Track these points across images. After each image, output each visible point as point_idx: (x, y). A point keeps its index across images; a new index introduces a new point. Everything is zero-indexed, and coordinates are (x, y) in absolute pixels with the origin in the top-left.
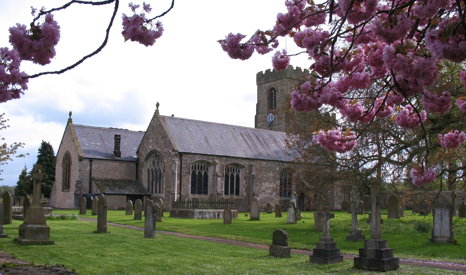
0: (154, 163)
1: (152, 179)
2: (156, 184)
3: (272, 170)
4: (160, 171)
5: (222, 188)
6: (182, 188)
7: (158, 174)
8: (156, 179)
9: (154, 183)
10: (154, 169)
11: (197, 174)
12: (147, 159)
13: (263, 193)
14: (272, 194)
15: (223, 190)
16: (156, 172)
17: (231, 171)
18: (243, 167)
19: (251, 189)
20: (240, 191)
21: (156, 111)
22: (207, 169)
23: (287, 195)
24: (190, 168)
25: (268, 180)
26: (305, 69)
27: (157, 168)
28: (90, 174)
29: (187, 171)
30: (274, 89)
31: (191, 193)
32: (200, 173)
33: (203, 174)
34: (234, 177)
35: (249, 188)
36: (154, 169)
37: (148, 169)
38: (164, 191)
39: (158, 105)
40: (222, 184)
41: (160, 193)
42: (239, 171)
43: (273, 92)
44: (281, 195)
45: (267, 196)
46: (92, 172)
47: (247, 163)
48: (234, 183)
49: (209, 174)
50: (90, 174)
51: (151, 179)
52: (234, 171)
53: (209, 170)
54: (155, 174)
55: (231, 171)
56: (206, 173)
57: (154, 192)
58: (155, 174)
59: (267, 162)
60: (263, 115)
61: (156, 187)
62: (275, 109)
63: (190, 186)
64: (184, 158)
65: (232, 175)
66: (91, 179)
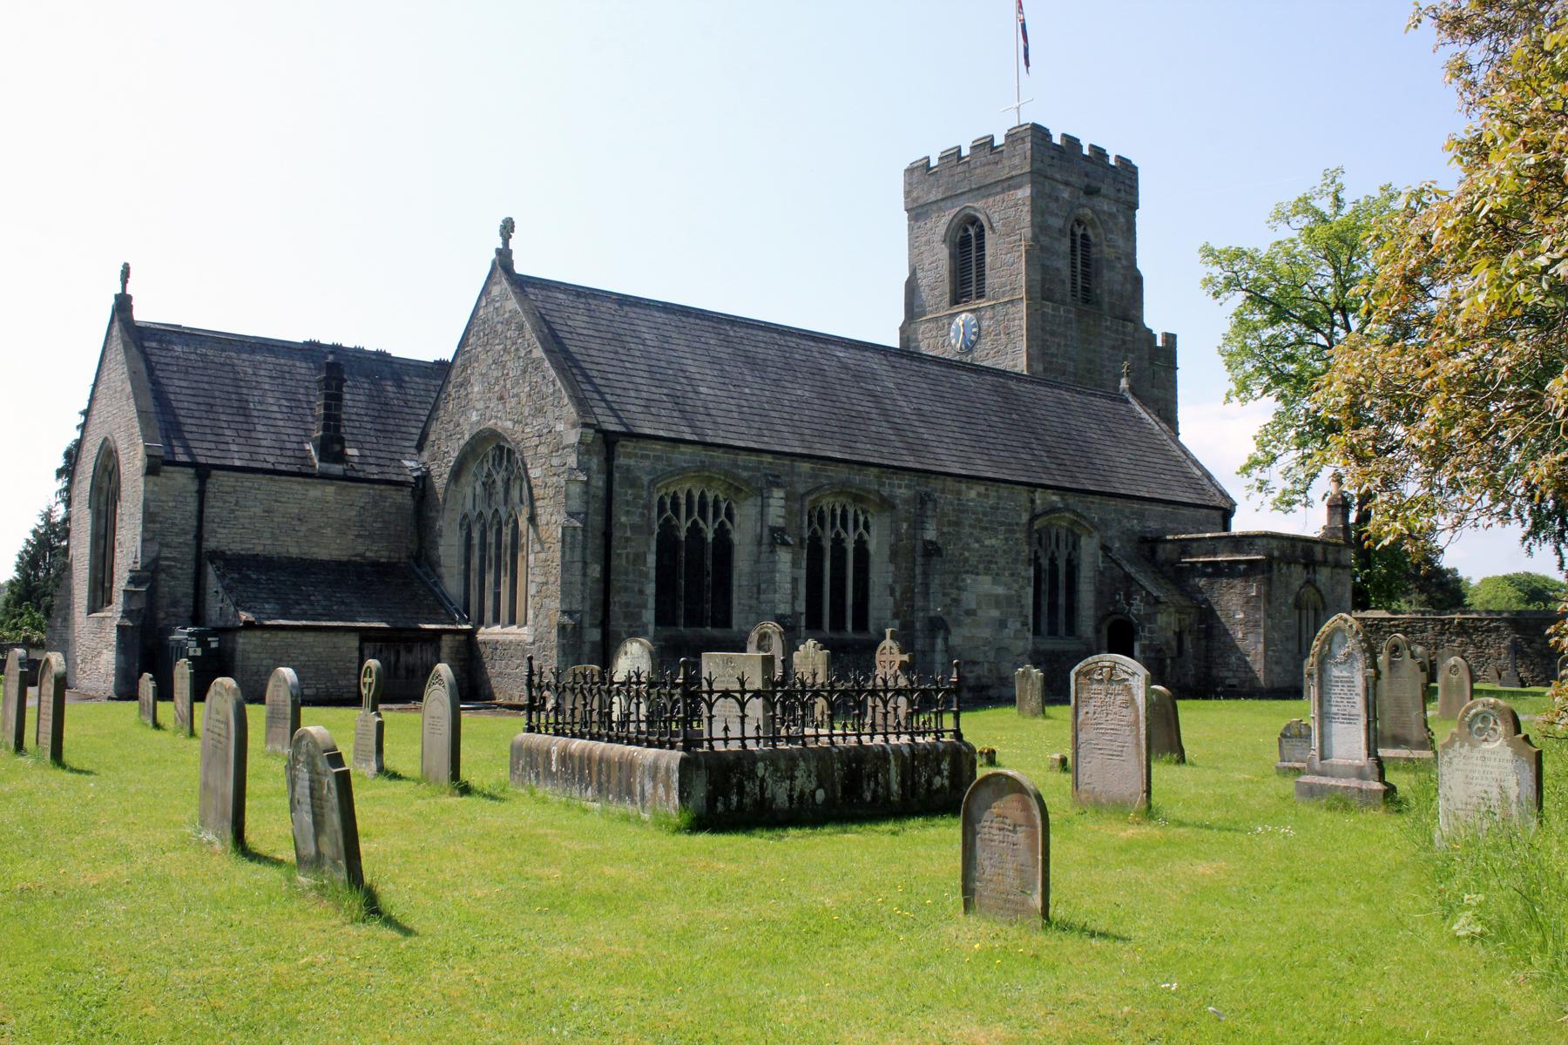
0: (488, 486)
1: (482, 559)
2: (497, 583)
3: (1002, 524)
4: (516, 522)
5: (794, 598)
6: (615, 599)
7: (507, 532)
8: (498, 557)
9: (490, 578)
10: (489, 514)
11: (683, 535)
12: (457, 473)
13: (968, 620)
14: (1002, 624)
15: (801, 607)
16: (499, 532)
17: (833, 525)
18: (887, 504)
19: (919, 603)
20: (873, 614)
21: (498, 252)
22: (729, 515)
23: (1062, 629)
24: (648, 507)
25: (987, 564)
26: (1092, 147)
27: (502, 510)
28: (199, 537)
29: (636, 519)
30: (974, 221)
31: (807, 627)
32: (695, 531)
33: (710, 536)
34: (844, 551)
35: (912, 599)
36: (489, 514)
37: (465, 516)
38: (531, 613)
39: (508, 228)
40: (795, 581)
41: (512, 621)
42: (866, 527)
43: (972, 232)
44: (1037, 631)
45: (986, 633)
46: (207, 527)
47: (902, 492)
48: (844, 579)
49: (736, 537)
50: (199, 537)
51: (475, 561)
52: (844, 526)
53: (737, 519)
54: (491, 538)
55: (833, 525)
56: (723, 535)
57: (489, 615)
58: (491, 538)
59: (982, 489)
60: (595, 717)
61: (497, 596)
62: (981, 295)
63: (651, 589)
64: (621, 461)
65: (838, 543)
66: (202, 558)
